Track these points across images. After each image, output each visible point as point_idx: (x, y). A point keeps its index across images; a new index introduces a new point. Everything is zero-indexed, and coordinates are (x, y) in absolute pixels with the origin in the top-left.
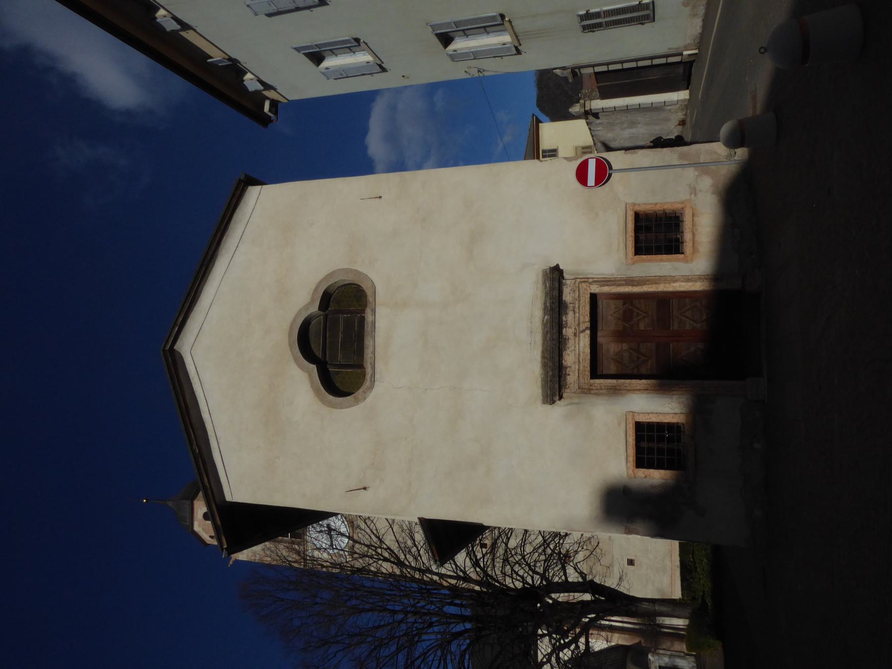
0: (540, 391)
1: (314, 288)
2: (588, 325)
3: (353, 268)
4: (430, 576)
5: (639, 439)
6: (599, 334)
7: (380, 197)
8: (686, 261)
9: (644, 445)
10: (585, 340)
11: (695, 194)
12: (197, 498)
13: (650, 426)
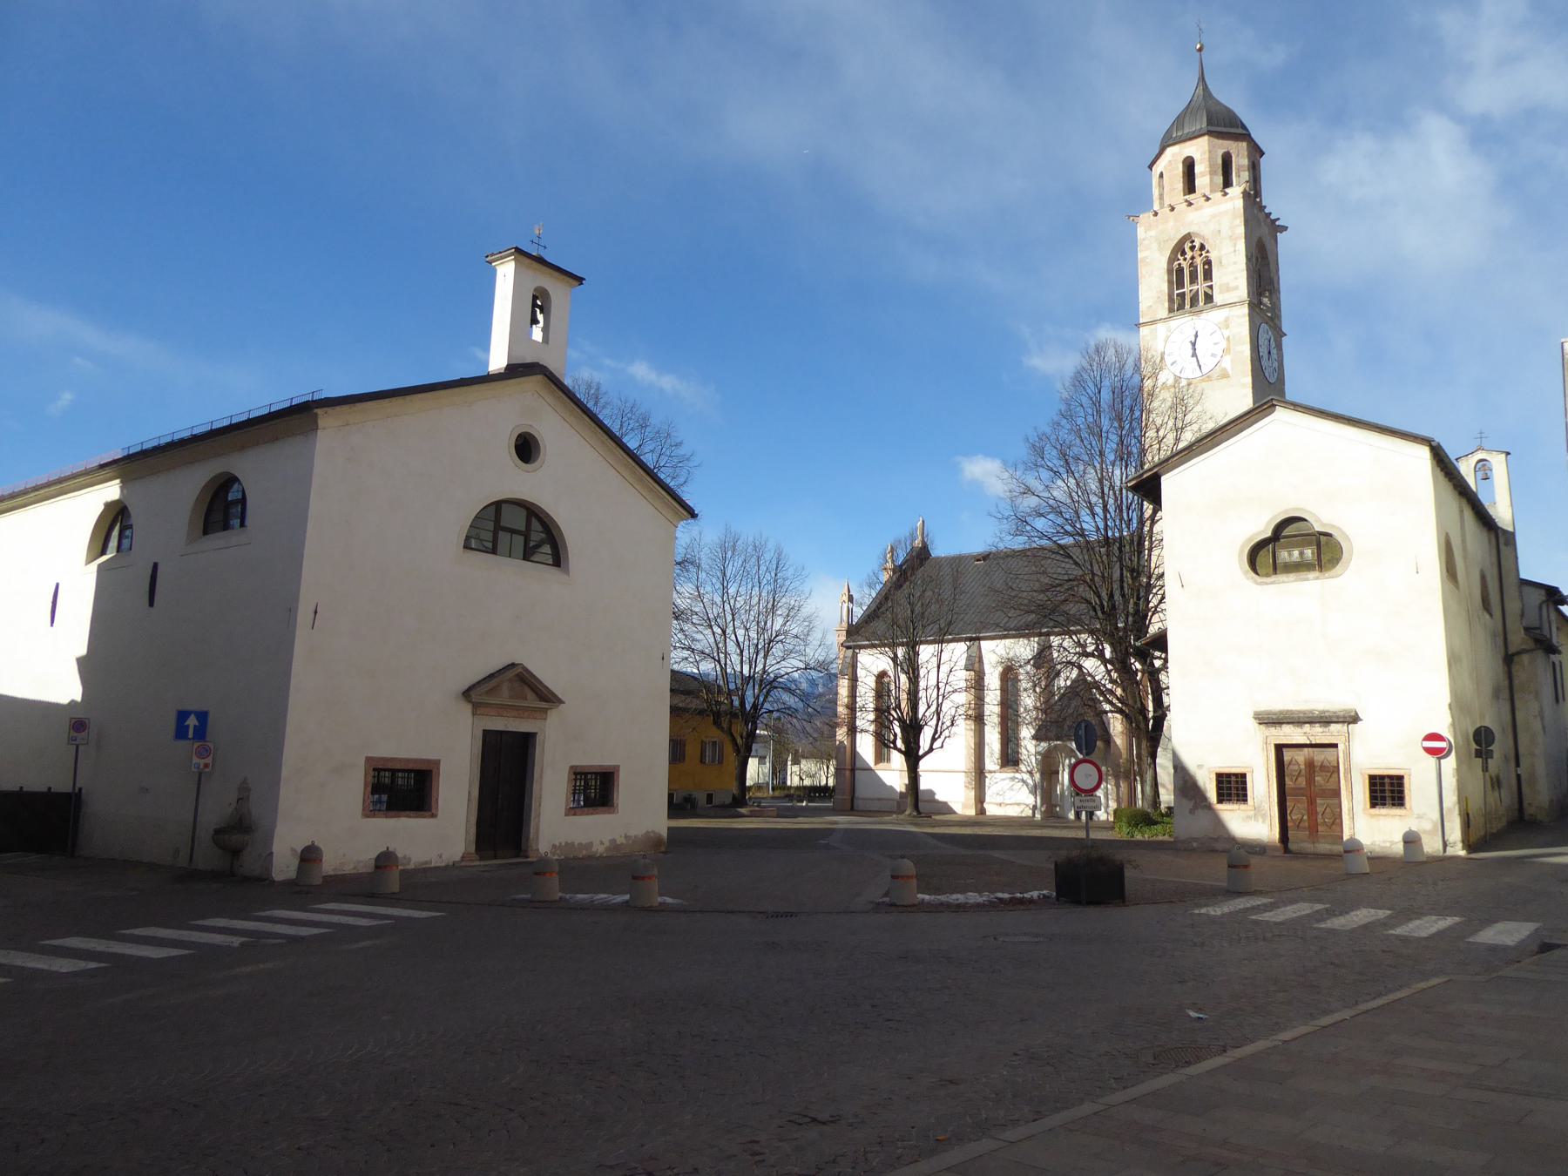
0: (1263, 709)
1: (1334, 524)
2: (1313, 742)
3: (1354, 557)
5: (1236, 775)
8: (1365, 809)
10: (1303, 740)
11: (1417, 818)
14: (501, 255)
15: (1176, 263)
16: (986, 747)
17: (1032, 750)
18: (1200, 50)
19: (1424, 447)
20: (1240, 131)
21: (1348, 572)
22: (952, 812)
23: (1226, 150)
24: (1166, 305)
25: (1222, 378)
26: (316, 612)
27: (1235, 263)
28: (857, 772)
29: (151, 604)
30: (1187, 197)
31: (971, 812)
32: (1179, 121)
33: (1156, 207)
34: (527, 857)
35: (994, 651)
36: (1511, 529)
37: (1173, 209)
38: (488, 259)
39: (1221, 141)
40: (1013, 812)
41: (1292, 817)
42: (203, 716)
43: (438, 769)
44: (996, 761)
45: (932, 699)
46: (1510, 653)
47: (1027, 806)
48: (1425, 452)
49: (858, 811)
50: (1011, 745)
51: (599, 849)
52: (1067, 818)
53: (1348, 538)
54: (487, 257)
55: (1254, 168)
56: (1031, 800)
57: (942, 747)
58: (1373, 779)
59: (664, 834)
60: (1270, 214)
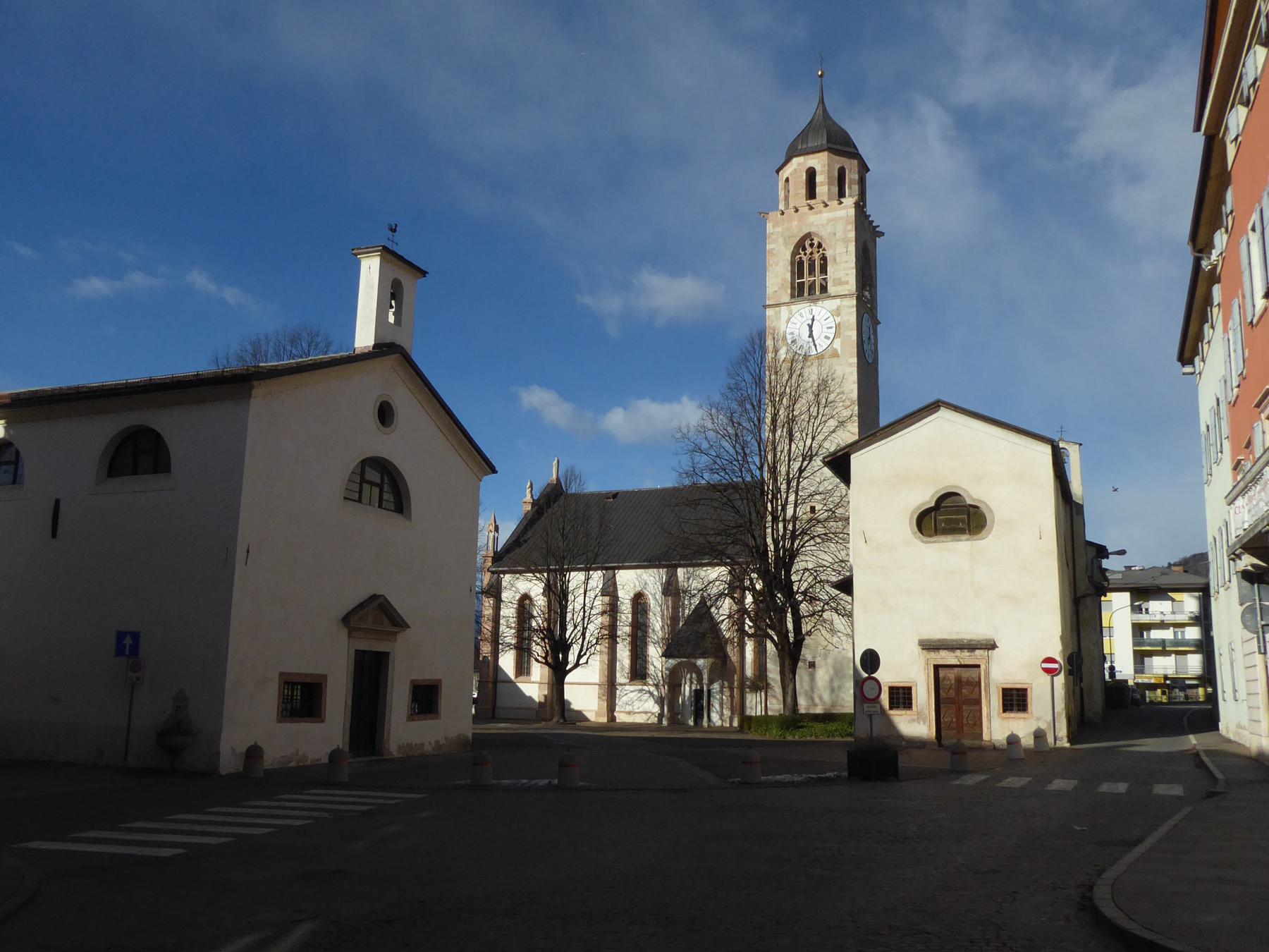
2: (963, 663)
4: (779, 512)
5: (903, 688)
6: (959, 669)
7: (1040, 538)
8: (999, 714)
9: (901, 691)
10: (955, 662)
12: (834, 156)
13: (910, 694)
14: (368, 250)
15: (798, 256)
16: (618, 664)
17: (659, 665)
18: (821, 76)
19: (1047, 445)
20: (852, 150)
21: (990, 536)
22: (586, 719)
23: (841, 165)
24: (789, 291)
25: (834, 357)
26: (248, 551)
27: (847, 262)
28: (498, 685)
29: (54, 535)
30: (809, 201)
31: (604, 720)
32: (803, 136)
33: (782, 207)
34: (383, 755)
35: (629, 580)
36: (1081, 503)
37: (797, 211)
38: (354, 252)
39: (837, 158)
40: (640, 719)
41: (945, 720)
42: (136, 636)
43: (326, 682)
44: (626, 675)
45: (578, 622)
46: (1078, 596)
47: (653, 714)
48: (1047, 450)
49: (497, 719)
50: (639, 661)
51: (428, 749)
52: (688, 725)
53: (991, 511)
54: (353, 250)
55: (862, 182)
56: (656, 709)
57: (587, 663)
58: (1005, 690)
59: (470, 736)
60: (870, 216)
